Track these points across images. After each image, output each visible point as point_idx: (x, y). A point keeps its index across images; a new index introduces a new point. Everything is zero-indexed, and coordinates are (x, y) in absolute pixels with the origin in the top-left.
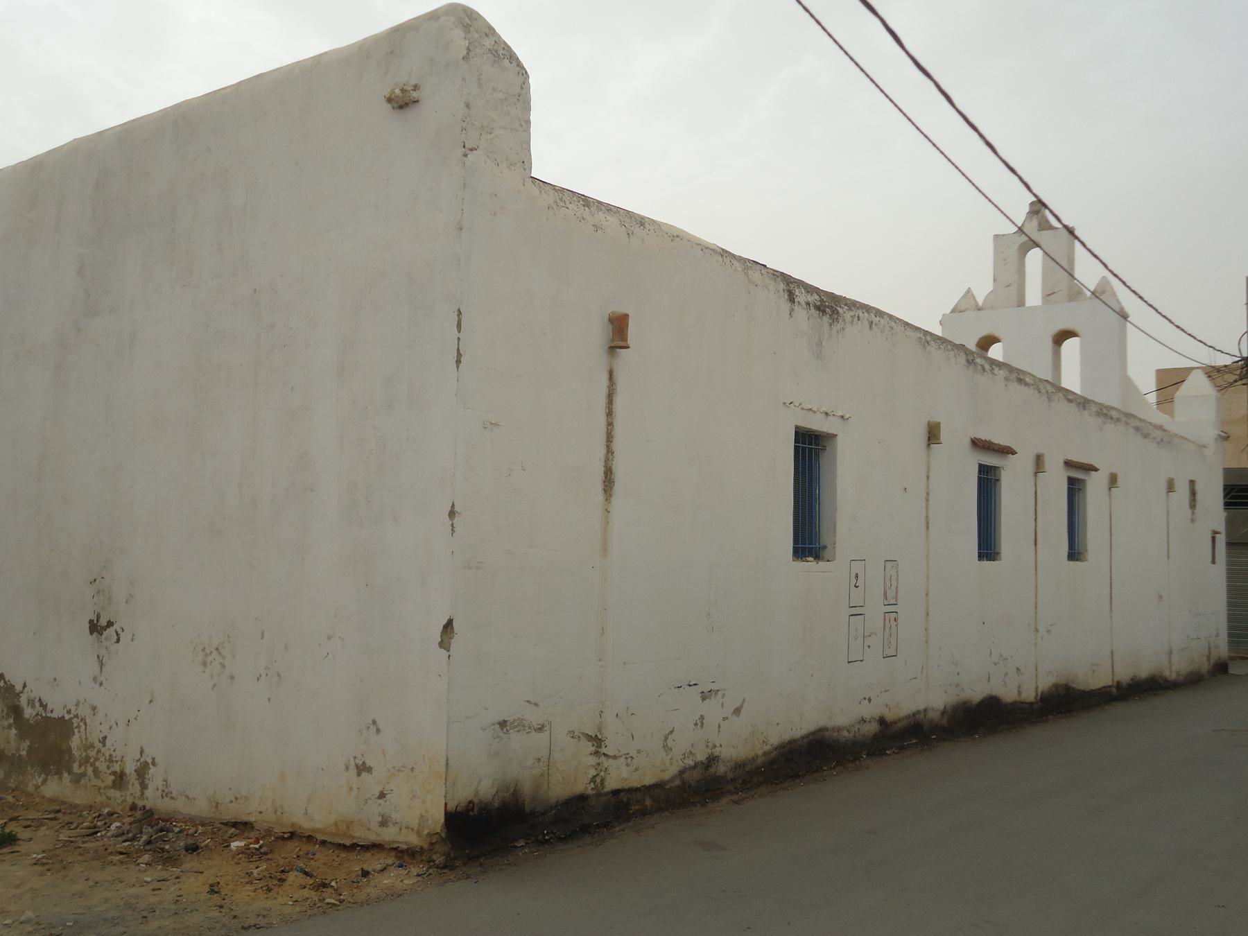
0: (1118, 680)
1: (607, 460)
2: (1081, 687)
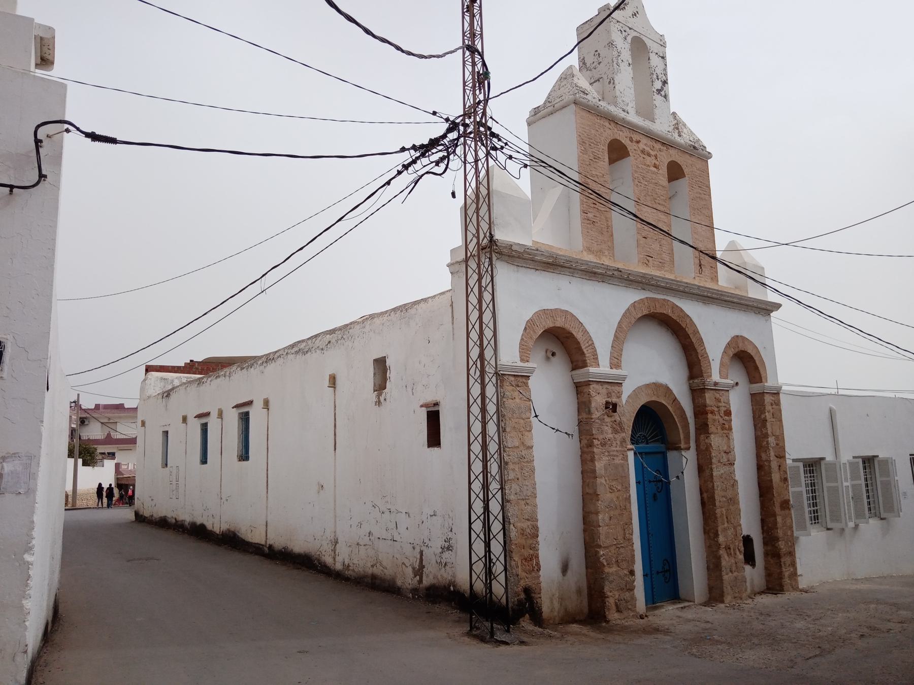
0: (271, 543)
1: (709, 256)
2: (243, 537)
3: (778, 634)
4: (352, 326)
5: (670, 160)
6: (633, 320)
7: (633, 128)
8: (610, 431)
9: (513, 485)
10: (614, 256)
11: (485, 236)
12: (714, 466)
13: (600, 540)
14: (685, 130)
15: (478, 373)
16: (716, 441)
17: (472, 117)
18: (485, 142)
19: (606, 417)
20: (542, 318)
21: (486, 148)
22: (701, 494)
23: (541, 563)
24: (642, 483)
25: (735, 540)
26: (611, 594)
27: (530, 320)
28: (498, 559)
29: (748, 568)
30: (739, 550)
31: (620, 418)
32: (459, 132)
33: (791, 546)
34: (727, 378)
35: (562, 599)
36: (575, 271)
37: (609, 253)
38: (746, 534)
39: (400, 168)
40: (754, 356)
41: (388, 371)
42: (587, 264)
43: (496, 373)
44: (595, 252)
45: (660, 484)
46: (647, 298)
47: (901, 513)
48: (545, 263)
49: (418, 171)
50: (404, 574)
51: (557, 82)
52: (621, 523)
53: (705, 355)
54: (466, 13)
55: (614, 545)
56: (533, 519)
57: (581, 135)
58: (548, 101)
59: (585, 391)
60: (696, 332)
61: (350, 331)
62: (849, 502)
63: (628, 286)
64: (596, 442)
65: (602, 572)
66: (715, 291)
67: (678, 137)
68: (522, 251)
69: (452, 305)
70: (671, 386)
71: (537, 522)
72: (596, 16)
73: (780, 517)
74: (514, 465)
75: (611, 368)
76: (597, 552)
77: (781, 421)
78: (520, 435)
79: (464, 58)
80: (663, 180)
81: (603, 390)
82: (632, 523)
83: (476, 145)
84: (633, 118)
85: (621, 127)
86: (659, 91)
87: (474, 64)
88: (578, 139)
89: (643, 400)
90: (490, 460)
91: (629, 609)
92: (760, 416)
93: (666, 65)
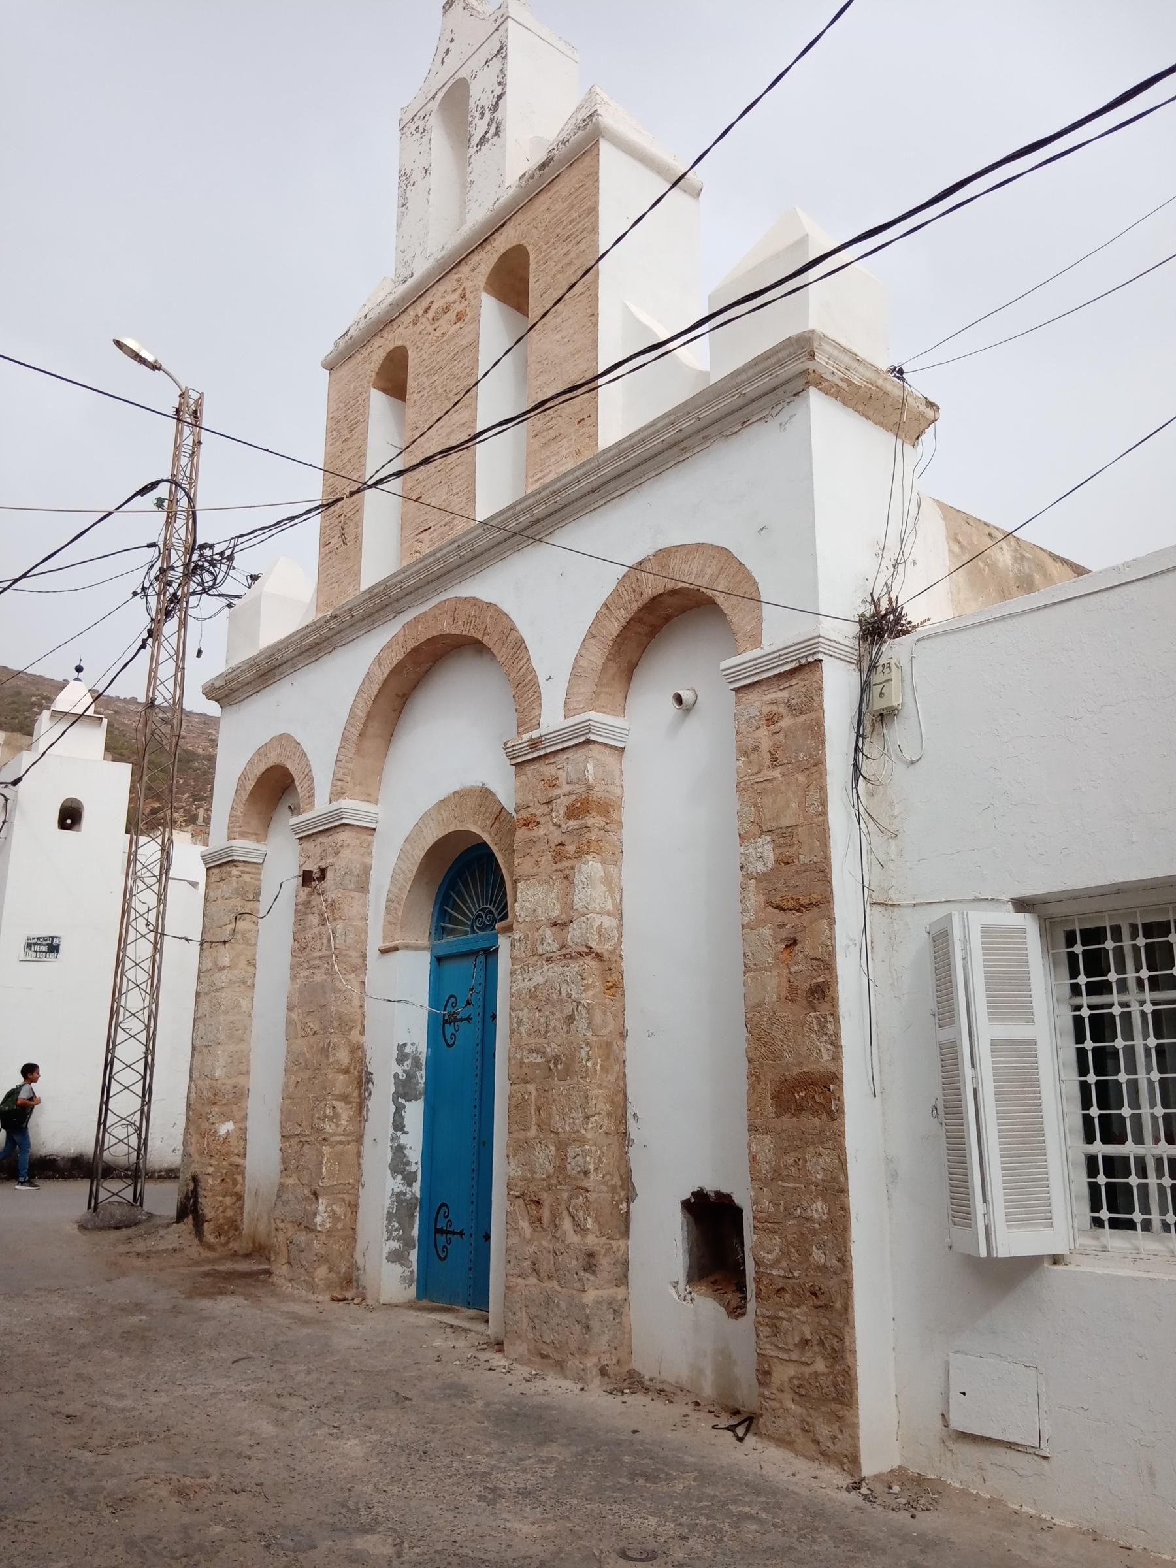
42: (292, 642)
52: (311, 1096)
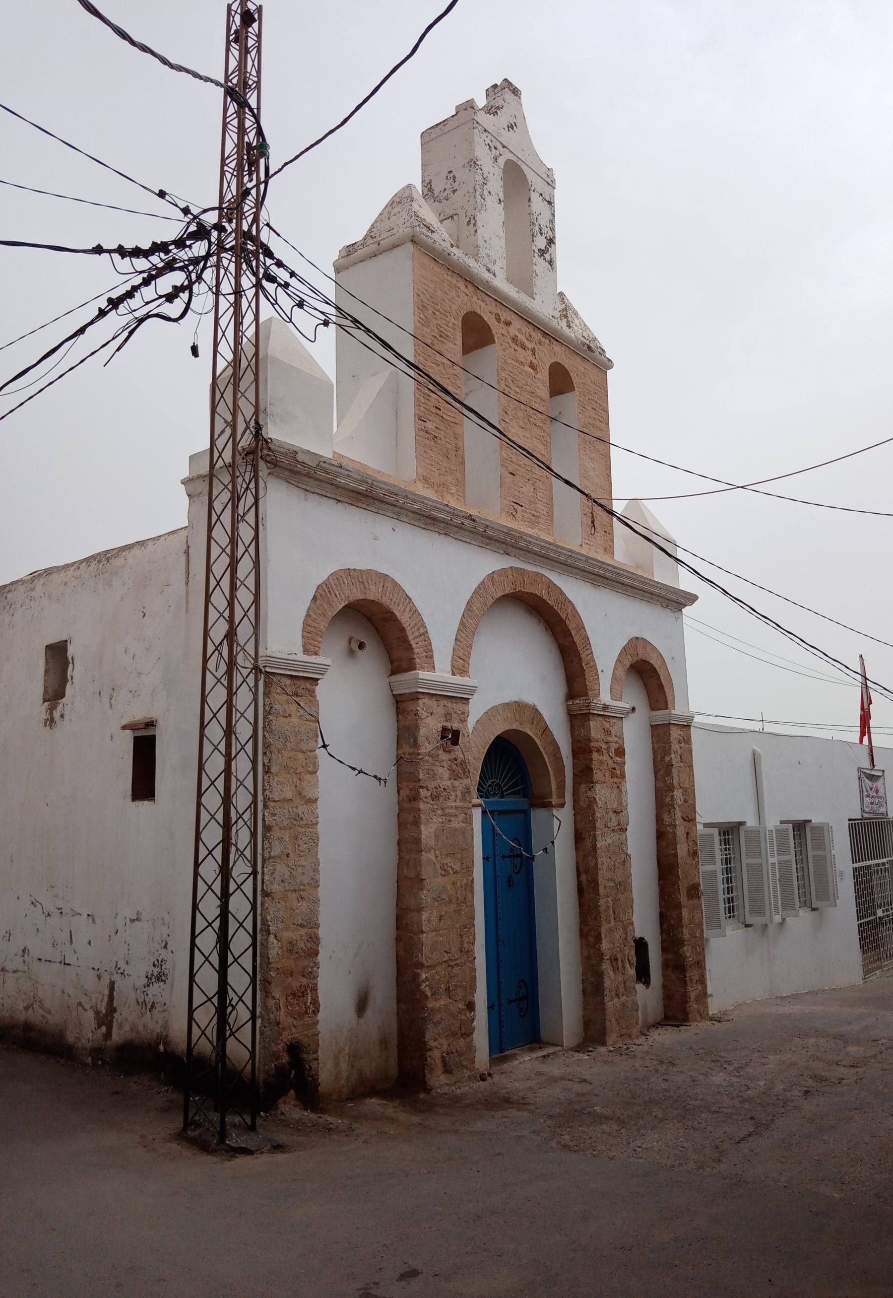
3: (689, 1097)
4: (13, 588)
5: (553, 361)
6: (490, 601)
7: (501, 301)
8: (446, 775)
9: (278, 867)
10: (464, 496)
11: (247, 427)
12: (598, 833)
13: (422, 955)
14: (576, 321)
15: (223, 668)
16: (602, 794)
17: (234, 221)
18: (254, 263)
19: (441, 752)
20: (344, 583)
21: (255, 274)
22: (579, 875)
23: (321, 1000)
24: (491, 860)
25: (625, 946)
26: (436, 1044)
27: (324, 585)
28: (240, 999)
29: (640, 987)
30: (629, 962)
31: (464, 756)
32: (210, 243)
33: (700, 953)
34: (620, 699)
35: (354, 1057)
36: (402, 511)
37: (457, 491)
38: (639, 937)
39: (103, 304)
40: (657, 669)
41: (71, 666)
42: (423, 503)
43: (256, 669)
44: (436, 487)
45: (517, 861)
46: (511, 567)
47: (837, 901)
48: (353, 491)
49: (135, 310)
50: (80, 1024)
51: (385, 208)
53: (592, 664)
54: (232, 44)
55: (445, 961)
56: (311, 924)
57: (420, 293)
58: (370, 235)
59: (410, 709)
60: (581, 627)
61: (9, 595)
62: (775, 887)
63: (484, 546)
64: (423, 793)
65: (423, 1009)
66: (610, 568)
67: (567, 328)
68: (315, 466)
69: (187, 552)
70: (541, 708)
71: (318, 928)
72: (453, 116)
73: (686, 909)
74: (283, 831)
75: (453, 674)
76: (417, 976)
77: (691, 766)
78: (296, 780)
79: (225, 118)
80: (543, 391)
81: (439, 708)
82: (474, 926)
83: (238, 268)
84: (501, 283)
85: (482, 294)
86: (542, 252)
87: (242, 131)
88: (416, 299)
89: (499, 729)
90: (236, 822)
91: (464, 1066)
92: (663, 759)
93: (553, 215)
